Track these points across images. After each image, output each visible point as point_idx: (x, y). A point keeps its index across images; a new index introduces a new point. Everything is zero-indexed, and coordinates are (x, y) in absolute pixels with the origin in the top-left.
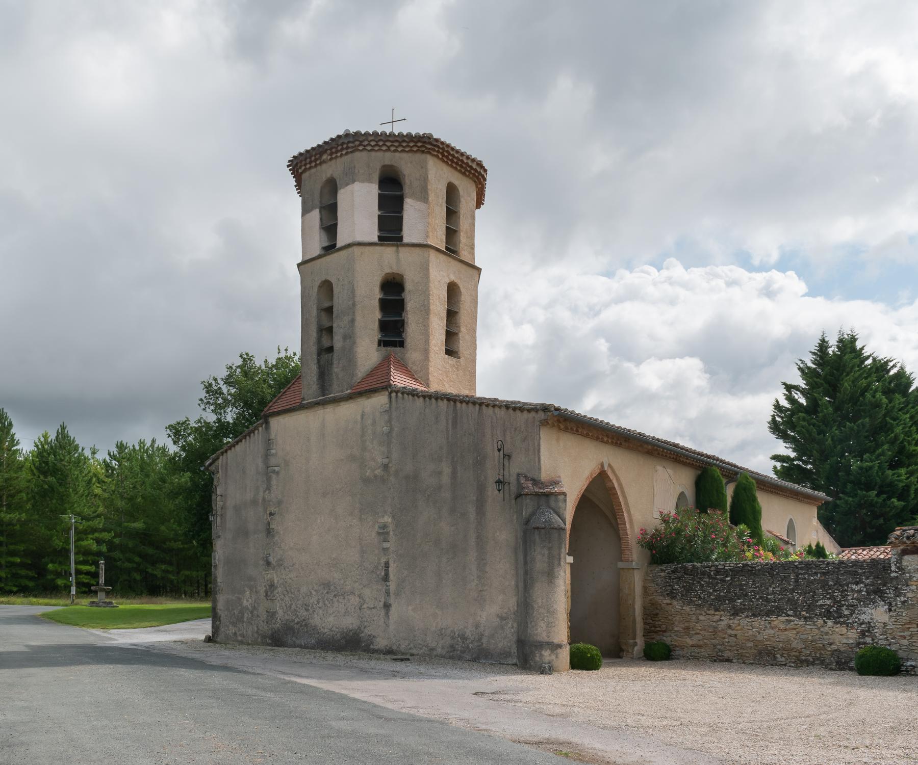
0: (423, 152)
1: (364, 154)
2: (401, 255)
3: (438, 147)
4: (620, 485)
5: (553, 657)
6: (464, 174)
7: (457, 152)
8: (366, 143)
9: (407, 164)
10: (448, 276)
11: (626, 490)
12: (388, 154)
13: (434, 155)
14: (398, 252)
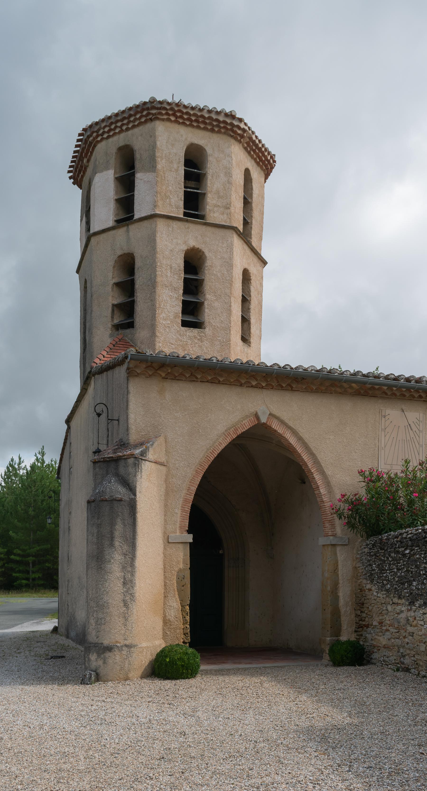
0: (151, 120)
1: (104, 143)
2: (131, 233)
3: (165, 109)
4: (300, 439)
5: (100, 662)
6: (212, 131)
7: (193, 108)
8: (101, 132)
9: (136, 138)
10: (185, 242)
11: (312, 445)
12: (122, 135)
13: (163, 120)
14: (128, 231)
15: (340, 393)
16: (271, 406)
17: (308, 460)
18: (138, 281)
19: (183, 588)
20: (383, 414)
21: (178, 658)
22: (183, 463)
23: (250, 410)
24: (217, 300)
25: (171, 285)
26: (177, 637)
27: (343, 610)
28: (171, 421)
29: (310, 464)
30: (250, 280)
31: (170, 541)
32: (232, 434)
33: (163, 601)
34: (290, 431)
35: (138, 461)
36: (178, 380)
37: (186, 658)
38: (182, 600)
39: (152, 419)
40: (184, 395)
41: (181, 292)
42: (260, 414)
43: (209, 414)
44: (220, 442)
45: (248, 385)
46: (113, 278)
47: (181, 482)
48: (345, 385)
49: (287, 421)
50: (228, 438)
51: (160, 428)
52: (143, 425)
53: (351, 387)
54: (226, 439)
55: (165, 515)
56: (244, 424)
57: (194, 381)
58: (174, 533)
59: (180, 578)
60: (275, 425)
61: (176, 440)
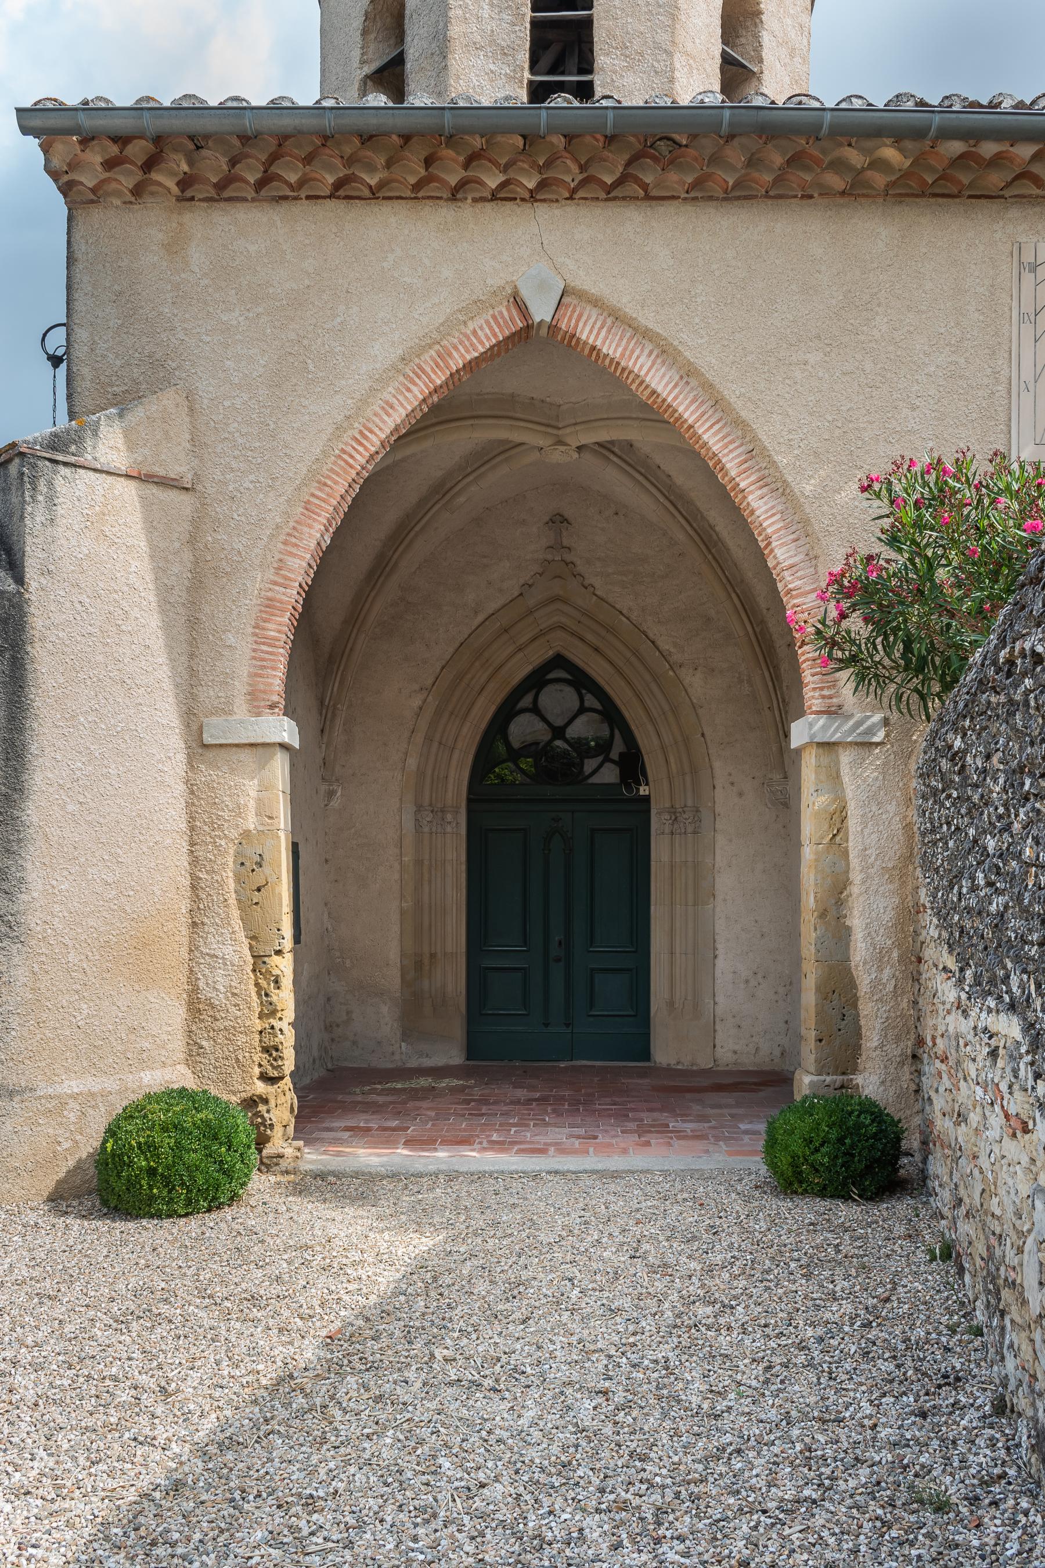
15: (843, 193)
16: (568, 261)
17: (726, 446)
18: (411, 51)
19: (256, 897)
20: (1028, 257)
21: (139, 1144)
22: (252, 477)
23: (489, 282)
24: (629, 68)
25: (493, 42)
26: (237, 1060)
27: (864, 981)
28: (208, 339)
29: (731, 462)
30: (760, 13)
31: (208, 739)
32: (428, 370)
33: (185, 940)
34: (649, 347)
35: (34, 466)
36: (229, 199)
37: (167, 1142)
38: (254, 938)
39: (144, 339)
40: (252, 248)
41: (524, 57)
42: (525, 293)
43: (342, 308)
44: (387, 403)
45: (477, 195)
46: (363, 62)
47: (244, 541)
48: (855, 157)
49: (631, 310)
50: (415, 384)
51: (174, 365)
52: (118, 363)
53: (880, 165)
54: (409, 390)
55: (192, 656)
56: (474, 332)
57: (285, 198)
58: (225, 713)
59: (247, 864)
60: (590, 330)
61: (227, 403)
